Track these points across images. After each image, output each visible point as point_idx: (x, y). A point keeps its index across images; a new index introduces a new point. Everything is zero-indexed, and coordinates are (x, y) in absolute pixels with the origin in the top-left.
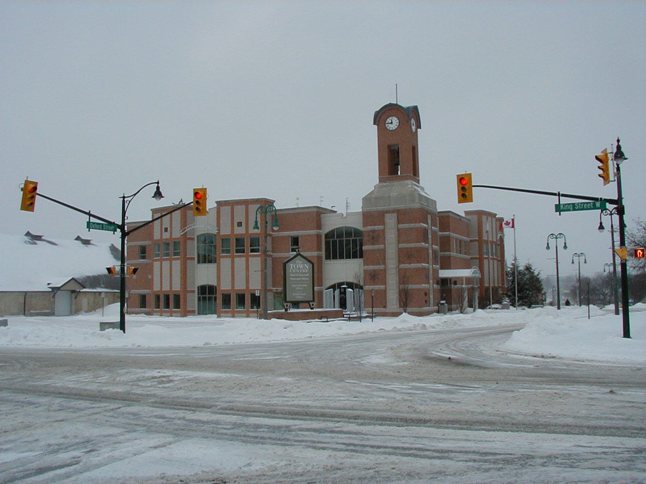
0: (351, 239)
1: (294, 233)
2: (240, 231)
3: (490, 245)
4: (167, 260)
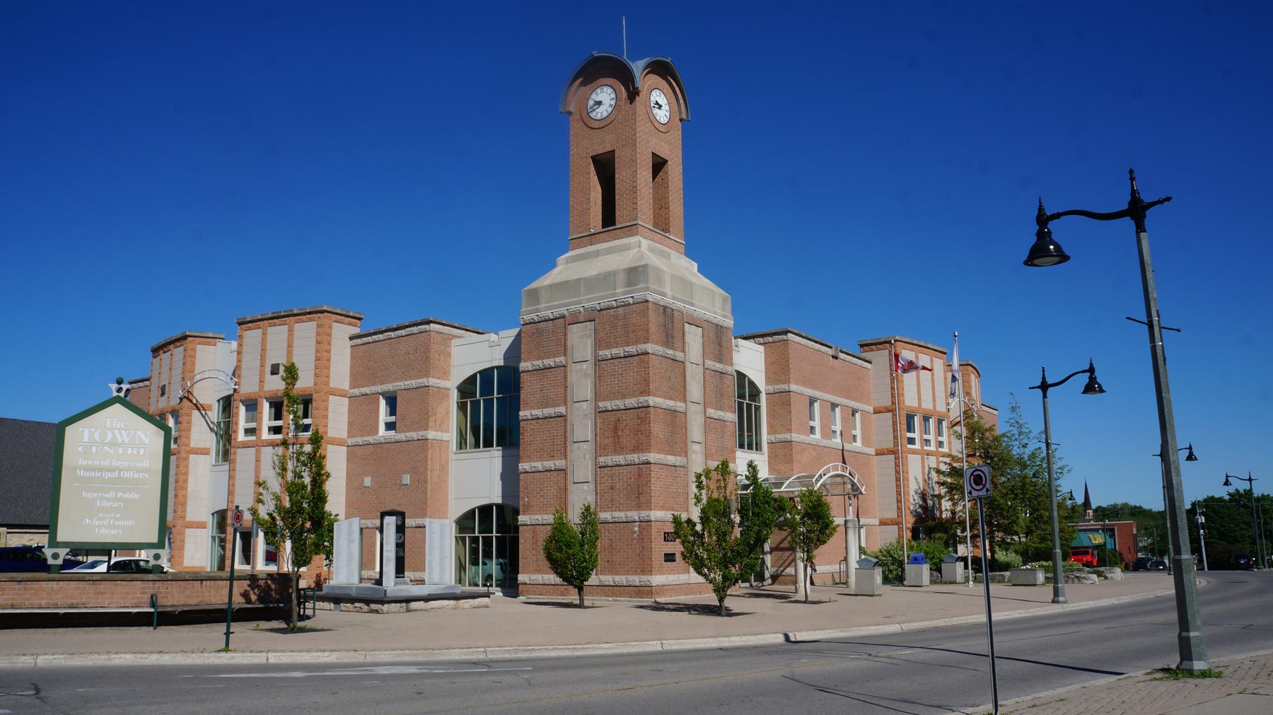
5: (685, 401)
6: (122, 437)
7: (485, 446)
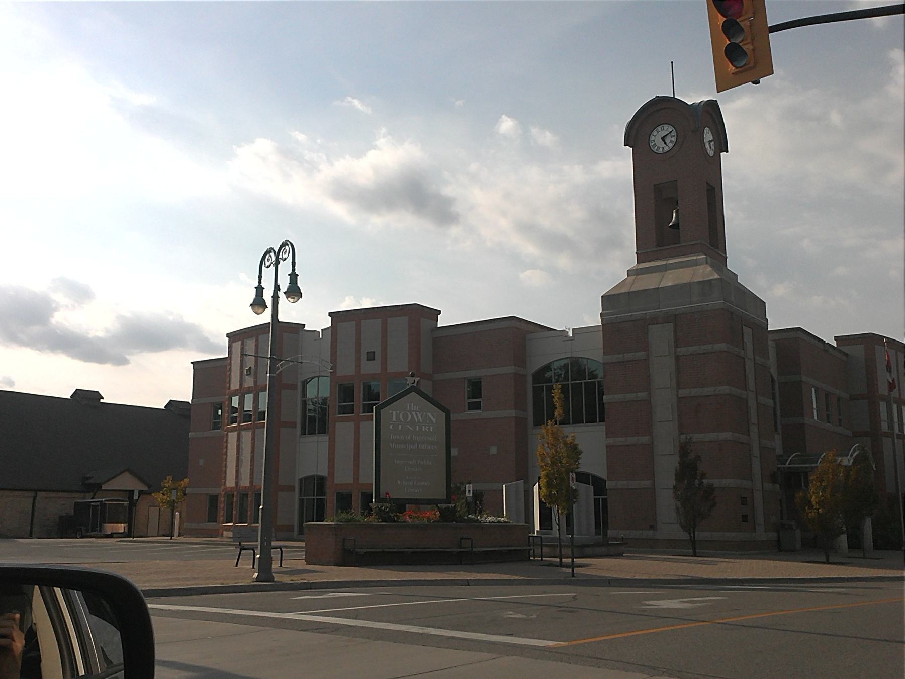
0: (587, 381)
1: (472, 374)
2: (371, 368)
3: (895, 407)
4: (247, 428)
5: (746, 390)
6: (418, 417)
7: (600, 422)
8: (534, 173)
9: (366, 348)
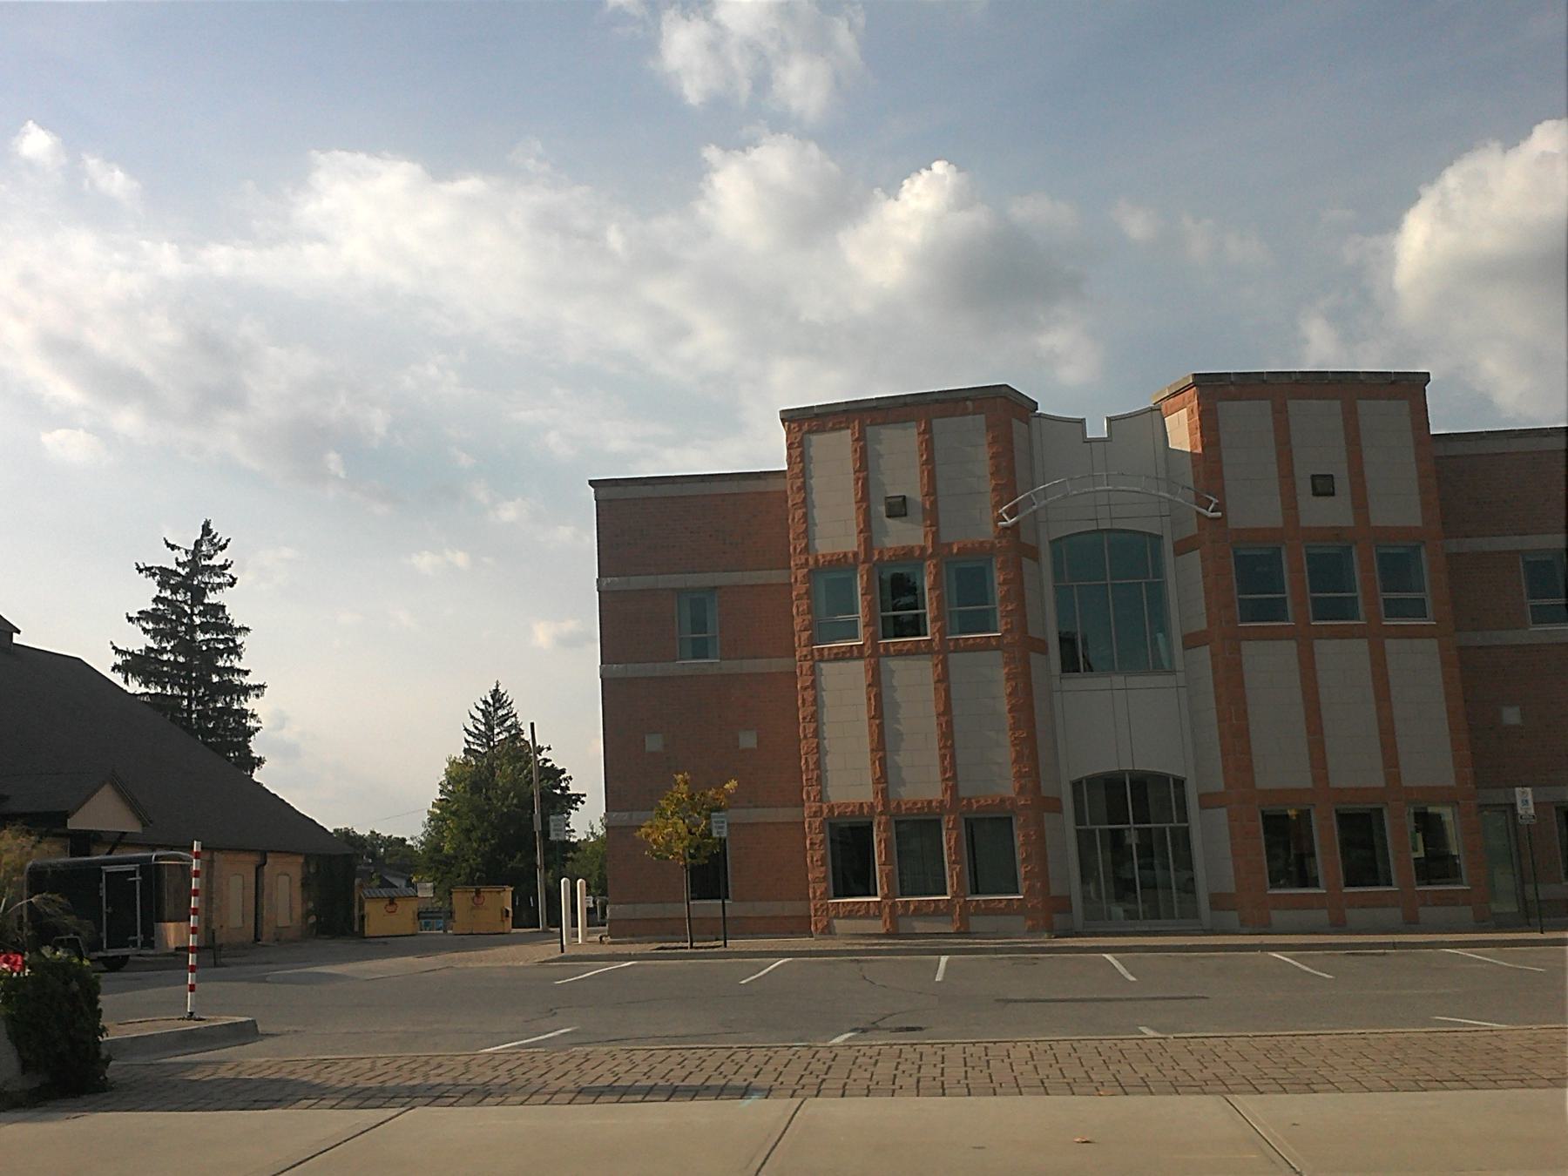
2: (903, 535)
8: (83, 244)
9: (1306, 466)
